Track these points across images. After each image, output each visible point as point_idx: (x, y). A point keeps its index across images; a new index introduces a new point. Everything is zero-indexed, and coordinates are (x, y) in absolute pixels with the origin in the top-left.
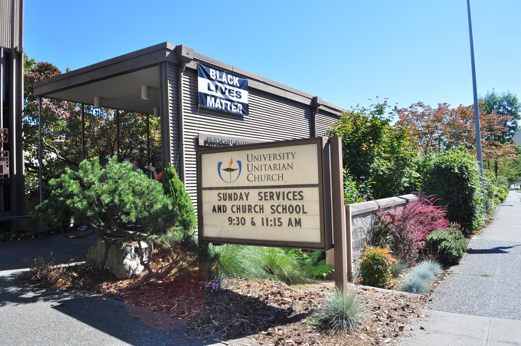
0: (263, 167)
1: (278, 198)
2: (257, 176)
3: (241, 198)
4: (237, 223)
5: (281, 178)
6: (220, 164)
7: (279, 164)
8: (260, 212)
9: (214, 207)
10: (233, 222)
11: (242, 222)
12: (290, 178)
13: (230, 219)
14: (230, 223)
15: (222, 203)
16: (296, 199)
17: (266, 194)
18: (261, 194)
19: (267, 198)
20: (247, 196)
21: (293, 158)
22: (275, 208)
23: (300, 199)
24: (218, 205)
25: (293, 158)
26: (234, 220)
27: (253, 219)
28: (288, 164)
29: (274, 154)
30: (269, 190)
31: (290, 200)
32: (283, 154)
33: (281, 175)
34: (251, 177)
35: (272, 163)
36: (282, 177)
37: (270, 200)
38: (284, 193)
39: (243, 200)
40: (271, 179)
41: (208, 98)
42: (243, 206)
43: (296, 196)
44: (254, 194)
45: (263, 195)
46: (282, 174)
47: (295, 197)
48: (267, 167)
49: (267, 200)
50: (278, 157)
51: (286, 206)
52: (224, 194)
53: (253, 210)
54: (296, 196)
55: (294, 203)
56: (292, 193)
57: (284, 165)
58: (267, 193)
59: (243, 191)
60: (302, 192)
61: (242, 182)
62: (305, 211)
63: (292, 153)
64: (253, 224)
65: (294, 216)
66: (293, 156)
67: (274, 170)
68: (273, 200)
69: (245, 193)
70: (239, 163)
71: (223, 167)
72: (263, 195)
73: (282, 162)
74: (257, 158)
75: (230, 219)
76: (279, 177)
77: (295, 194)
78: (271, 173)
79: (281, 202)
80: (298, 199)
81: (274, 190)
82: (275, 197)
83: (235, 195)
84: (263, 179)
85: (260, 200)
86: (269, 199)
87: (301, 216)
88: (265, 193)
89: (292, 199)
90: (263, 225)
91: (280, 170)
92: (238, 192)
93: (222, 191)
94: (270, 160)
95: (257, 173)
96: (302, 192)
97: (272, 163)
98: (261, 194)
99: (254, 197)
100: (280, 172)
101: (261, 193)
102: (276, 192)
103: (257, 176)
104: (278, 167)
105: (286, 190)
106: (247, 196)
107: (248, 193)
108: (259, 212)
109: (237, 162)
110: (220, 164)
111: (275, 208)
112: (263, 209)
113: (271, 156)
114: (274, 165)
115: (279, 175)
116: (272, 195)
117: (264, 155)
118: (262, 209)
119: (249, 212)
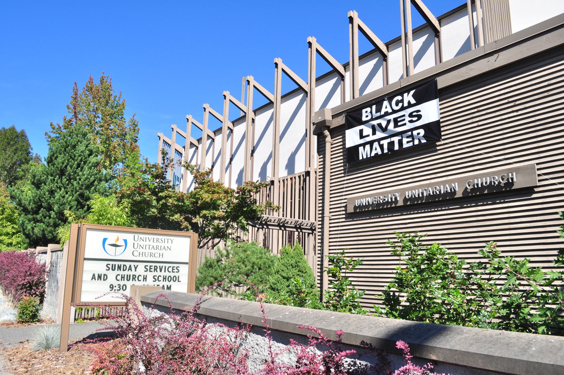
0: (147, 247)
1: (161, 271)
2: (141, 253)
3: (130, 268)
4: (119, 289)
5: (161, 256)
6: (105, 240)
8: (121, 280)
9: (94, 275)
10: (114, 288)
13: (112, 286)
14: (111, 289)
16: (174, 272)
18: (146, 267)
19: (151, 270)
20: (136, 268)
23: (177, 272)
24: (99, 274)
26: (115, 287)
30: (154, 264)
33: (161, 254)
34: (136, 253)
35: (155, 244)
37: (154, 271)
38: (165, 267)
39: (131, 271)
41: (361, 149)
42: (127, 275)
43: (174, 269)
44: (141, 266)
47: (174, 271)
49: (152, 271)
50: (160, 241)
52: (112, 265)
53: (136, 279)
54: (174, 269)
55: (172, 275)
56: (172, 267)
58: (152, 266)
59: (132, 264)
60: (179, 267)
62: (179, 280)
68: (157, 271)
69: (134, 266)
70: (125, 241)
71: (107, 242)
72: (148, 268)
73: (163, 245)
75: (112, 286)
77: (174, 268)
78: (153, 251)
79: (163, 274)
81: (158, 265)
82: (158, 270)
83: (125, 267)
84: (146, 255)
86: (153, 271)
88: (150, 266)
92: (128, 264)
93: (111, 263)
95: (141, 250)
96: (179, 267)
100: (161, 252)
101: (147, 266)
102: (160, 267)
103: (141, 253)
104: (159, 248)
105: (167, 265)
106: (136, 268)
107: (137, 266)
108: (120, 280)
110: (105, 240)
112: (146, 279)
116: (156, 268)
118: (145, 278)
119: (133, 280)
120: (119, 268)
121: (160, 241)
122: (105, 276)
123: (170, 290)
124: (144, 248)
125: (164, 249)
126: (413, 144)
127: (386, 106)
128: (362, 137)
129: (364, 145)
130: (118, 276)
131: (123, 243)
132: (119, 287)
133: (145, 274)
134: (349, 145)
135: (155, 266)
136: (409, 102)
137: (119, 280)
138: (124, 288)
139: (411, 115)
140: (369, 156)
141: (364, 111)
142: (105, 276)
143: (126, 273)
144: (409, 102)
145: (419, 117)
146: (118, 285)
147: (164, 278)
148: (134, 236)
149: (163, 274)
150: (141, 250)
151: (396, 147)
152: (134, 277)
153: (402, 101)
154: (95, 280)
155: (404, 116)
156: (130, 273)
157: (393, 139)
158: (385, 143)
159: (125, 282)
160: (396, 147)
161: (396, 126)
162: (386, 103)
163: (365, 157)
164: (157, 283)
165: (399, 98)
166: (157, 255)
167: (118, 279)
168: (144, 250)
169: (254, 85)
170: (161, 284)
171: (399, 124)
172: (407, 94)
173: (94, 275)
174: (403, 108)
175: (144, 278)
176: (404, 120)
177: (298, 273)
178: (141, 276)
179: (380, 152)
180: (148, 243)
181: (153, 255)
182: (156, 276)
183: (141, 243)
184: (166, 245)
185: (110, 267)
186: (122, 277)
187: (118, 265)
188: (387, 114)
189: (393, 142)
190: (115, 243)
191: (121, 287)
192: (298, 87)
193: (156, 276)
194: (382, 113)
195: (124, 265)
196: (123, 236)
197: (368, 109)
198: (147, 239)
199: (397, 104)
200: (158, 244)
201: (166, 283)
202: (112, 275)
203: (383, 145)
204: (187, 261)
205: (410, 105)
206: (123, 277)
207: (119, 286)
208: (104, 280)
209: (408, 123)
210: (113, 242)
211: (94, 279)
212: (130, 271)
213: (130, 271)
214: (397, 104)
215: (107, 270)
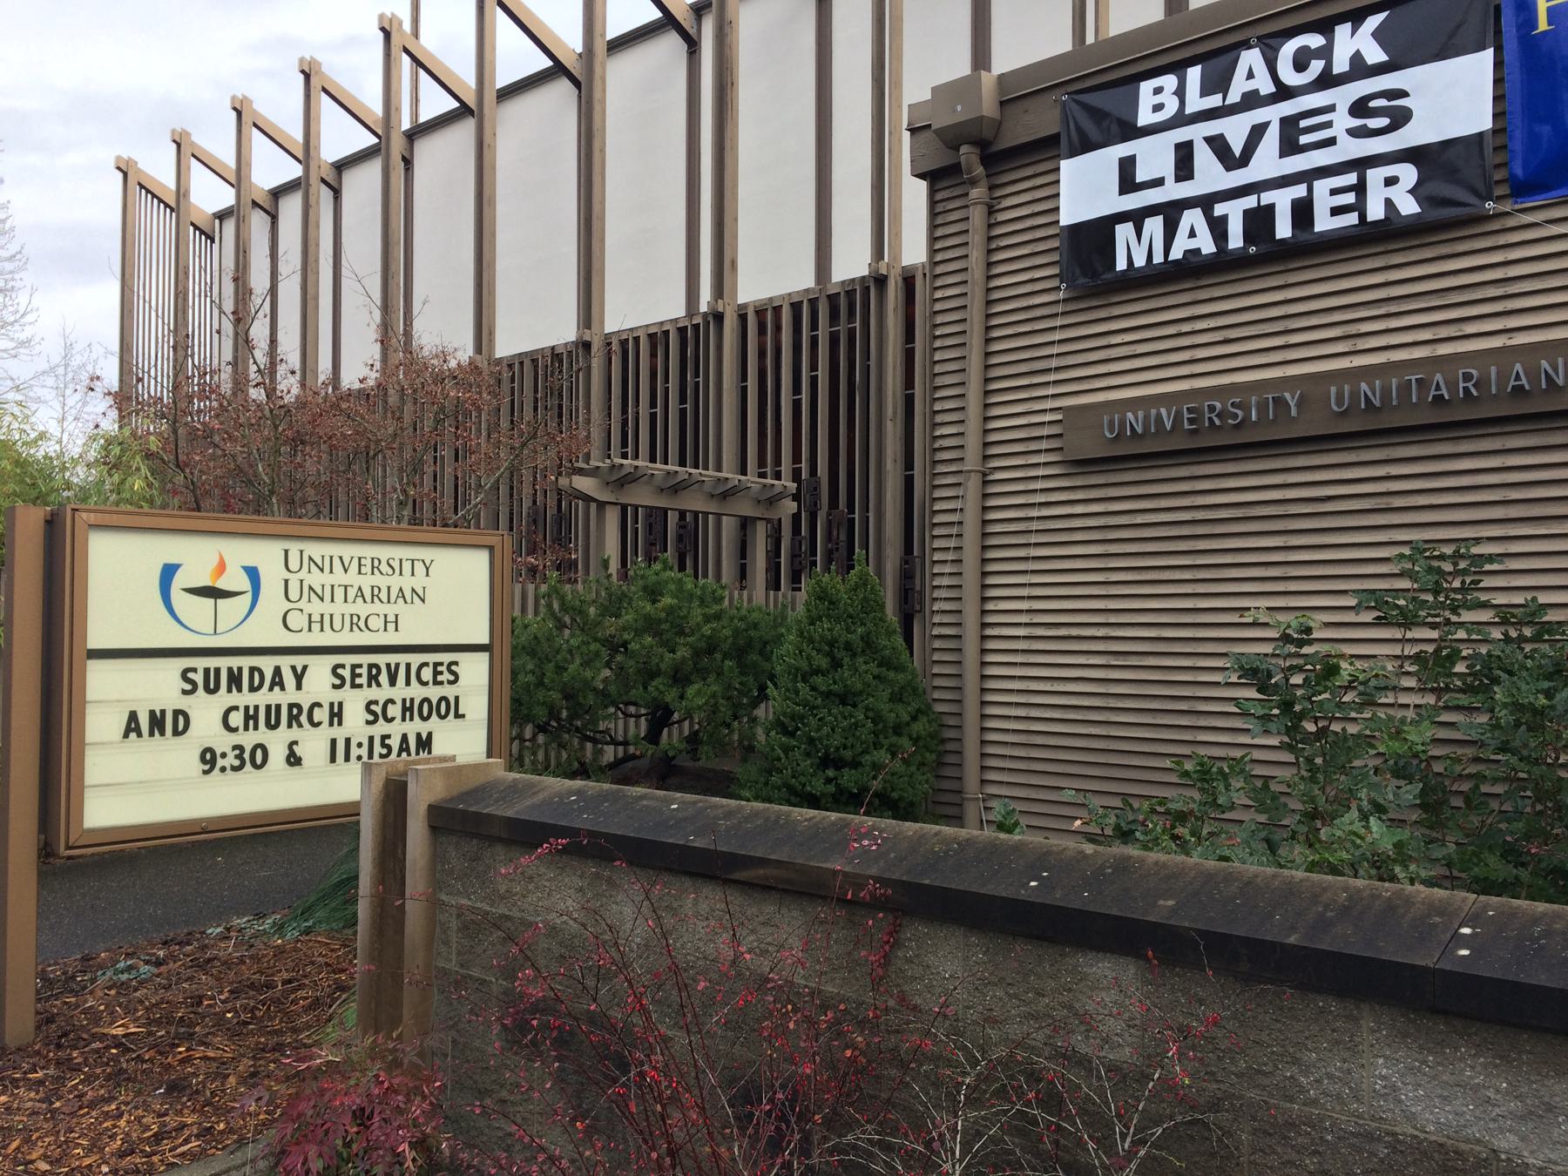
0: (339, 593)
1: (393, 682)
2: (316, 618)
3: (278, 681)
4: (237, 763)
5: (391, 627)
6: (169, 572)
7: (389, 588)
8: (246, 728)
9: (133, 717)
10: (220, 762)
11: (257, 758)
13: (208, 756)
14: (207, 767)
16: (441, 683)
17: (358, 671)
18: (340, 671)
19: (358, 681)
21: (427, 575)
22: (378, 709)
24: (152, 713)
25: (427, 575)
27: (295, 747)
28: (413, 590)
29: (373, 559)
31: (426, 684)
32: (401, 560)
33: (391, 618)
34: (296, 620)
35: (367, 582)
36: (396, 622)
37: (370, 685)
38: (408, 666)
39: (283, 688)
40: (363, 627)
41: (1124, 232)
42: (268, 707)
43: (441, 673)
45: (346, 673)
46: (397, 616)
47: (440, 678)
48: (352, 593)
49: (360, 686)
50: (384, 568)
51: (412, 700)
52: (207, 671)
54: (441, 673)
55: (434, 693)
56: (431, 665)
57: (401, 589)
58: (360, 666)
59: (285, 662)
60: (456, 663)
61: (264, 630)
63: (423, 561)
64: (293, 760)
66: (427, 569)
67: (373, 602)
69: (294, 668)
70: (253, 574)
71: (180, 581)
72: (346, 673)
73: (395, 582)
74: (320, 565)
75: (208, 756)
76: (386, 622)
77: (439, 669)
78: (362, 609)
79: (400, 692)
80: (446, 682)
81: (381, 659)
82: (384, 678)
84: (337, 626)
85: (335, 687)
86: (365, 685)
88: (354, 667)
89: (431, 683)
90: (333, 759)
91: (389, 602)
92: (267, 664)
93: (201, 663)
94: (360, 573)
95: (316, 607)
96: (456, 663)
97: (367, 582)
98: (340, 671)
99: (319, 682)
100: (390, 610)
101: (194, 670)
102: (388, 665)
103: (316, 618)
104: (384, 596)
105: (416, 659)
109: (242, 570)
110: (169, 572)
111: (378, 709)
112: (339, 715)
113: (363, 561)
114: (373, 587)
115: (386, 616)
116: (374, 671)
117: (341, 558)
118: (336, 715)
119: (290, 726)
120: (235, 680)
121: (384, 568)
122: (181, 719)
123: (430, 752)
124: (327, 597)
126: (1362, 216)
127: (1250, 69)
128: (1128, 184)
129: (1137, 217)
131: (243, 583)
132: (236, 757)
133: (336, 696)
134: (1072, 212)
136: (1357, 58)
137: (235, 730)
138: (259, 760)
139: (1360, 108)
140: (1158, 258)
141: (1146, 87)
142: (181, 719)
143: (263, 698)
144: (1357, 58)
145: (1400, 118)
146: (235, 748)
147: (404, 709)
148: (286, 552)
149: (400, 692)
150: (316, 607)
151: (1284, 230)
152: (295, 711)
153: (1326, 52)
154: (140, 735)
155: (1331, 109)
156: (276, 697)
157: (1267, 198)
158: (1234, 212)
159: (262, 735)
160: (1284, 230)
161: (1289, 146)
162: (1251, 58)
163: (1140, 261)
164: (381, 728)
165: (1315, 41)
166: (376, 623)
168: (326, 608)
169: (404, 47)
170: (396, 730)
171: (1304, 140)
172: (1348, 26)
173: (133, 717)
174: (1327, 81)
175: (332, 715)
176: (1329, 125)
177: (876, 671)
178: (319, 705)
179: (1207, 246)
180: (339, 577)
183: (316, 579)
184: (407, 582)
185: (199, 678)
186: (247, 717)
187: (230, 670)
188: (1252, 101)
189: (1271, 208)
190: (208, 583)
191: (247, 756)
192: (549, 63)
193: (376, 702)
194: (1234, 96)
195: (252, 670)
196: (241, 552)
197: (1169, 81)
198: (337, 563)
199: (1300, 65)
200: (377, 580)
201: (415, 727)
202: (206, 712)
203: (1224, 219)
204: (485, 640)
205: (1360, 69)
206: (251, 717)
207: (237, 752)
208: (176, 733)
209: (1344, 141)
210: (204, 581)
211: (133, 735)
212: (277, 689)
213: (277, 689)
214: (1300, 65)
215: (185, 692)
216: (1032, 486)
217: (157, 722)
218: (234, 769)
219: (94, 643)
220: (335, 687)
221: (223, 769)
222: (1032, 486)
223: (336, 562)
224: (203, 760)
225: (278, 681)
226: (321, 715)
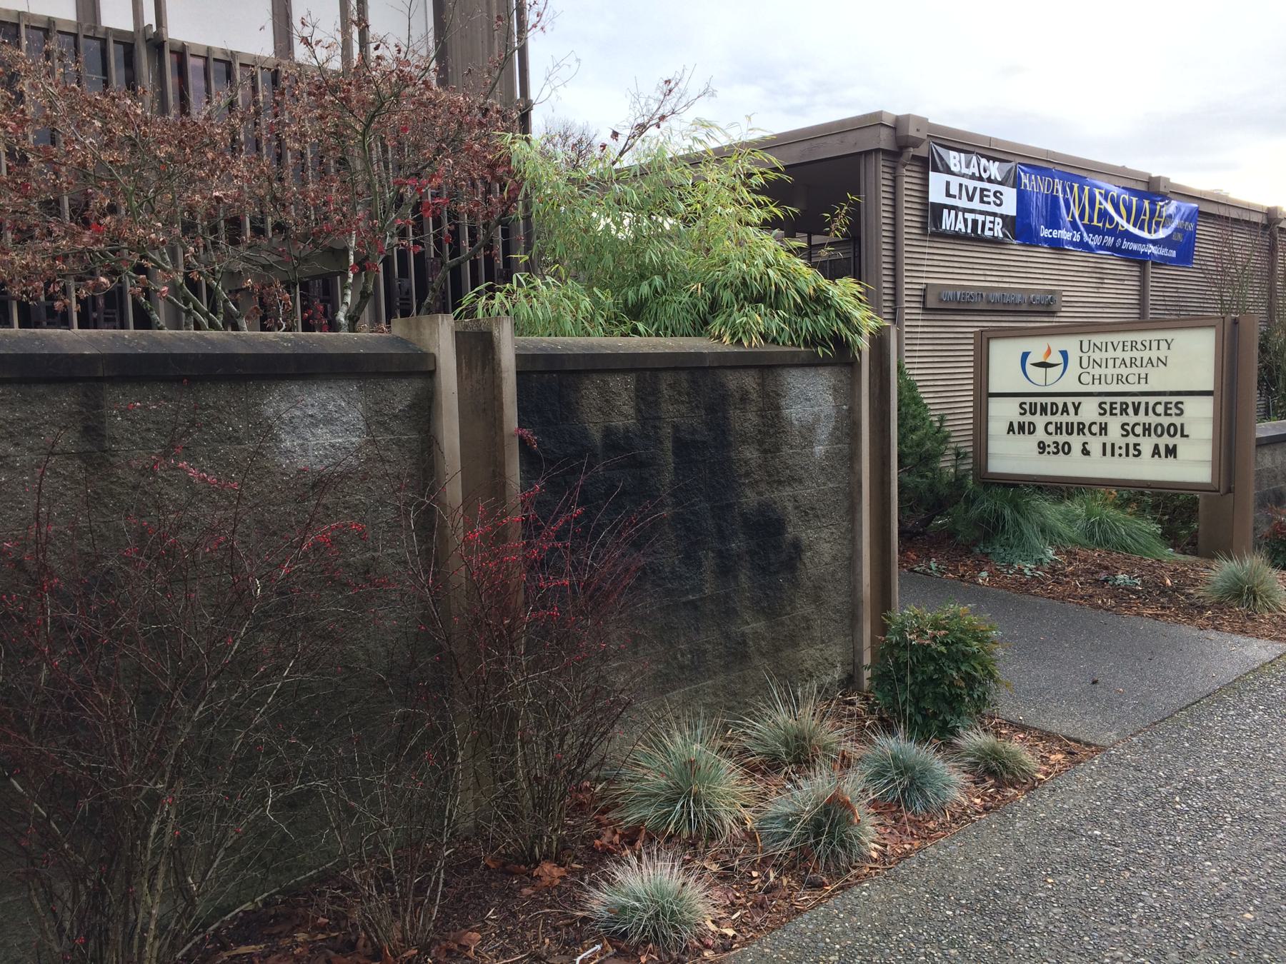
0: (1111, 363)
1: (1136, 413)
2: (1097, 377)
3: (1065, 410)
5: (1143, 381)
6: (1025, 356)
8: (1101, 434)
9: (1011, 424)
10: (1047, 449)
11: (1066, 449)
12: (1159, 380)
15: (1028, 418)
16: (1171, 415)
19: (1114, 411)
22: (1129, 428)
23: (1176, 415)
30: (1119, 399)
33: (1143, 376)
35: (1127, 356)
37: (1121, 414)
38: (1147, 403)
41: (945, 212)
42: (1067, 423)
45: (1027, 407)
47: (1169, 412)
50: (1139, 346)
51: (1150, 424)
52: (1031, 404)
55: (1166, 421)
59: (1069, 400)
60: (1182, 403)
61: (1069, 383)
64: (1086, 452)
65: (1166, 440)
69: (1073, 404)
70: (1064, 354)
71: (1030, 360)
72: (1107, 407)
73: (1146, 355)
78: (1124, 371)
81: (1129, 400)
82: (1130, 410)
84: (1109, 381)
87: (1177, 440)
88: (1112, 404)
90: (1104, 454)
92: (1060, 401)
95: (1097, 371)
96: (1182, 403)
100: (1143, 371)
101: (1105, 403)
102: (1133, 403)
103: (1097, 377)
104: (1138, 363)
105: (1152, 400)
110: (1025, 356)
111: (1129, 428)
112: (1105, 429)
118: (1104, 429)
121: (1139, 346)
124: (1104, 365)
125: (1150, 365)
130: (1049, 426)
131: (1060, 359)
135: (1122, 404)
146: (1054, 443)
150: (1097, 371)
154: (1160, 456)
167: (1050, 431)
168: (1103, 371)
173: (1011, 424)
181: (1124, 380)
182: (1128, 424)
183: (1097, 356)
184: (1154, 354)
185: (1027, 407)
186: (1057, 428)
191: (1060, 447)
193: (1128, 424)
198: (1110, 346)
200: (1135, 354)
204: (1210, 387)
210: (1041, 360)
211: (1156, 456)
216: (914, 342)
217: (1021, 427)
218: (1054, 453)
219: (992, 390)
220: (1100, 414)
221: (1049, 453)
222: (914, 342)
223: (1109, 345)
224: (1039, 447)
225: (1065, 410)
226: (1095, 429)
